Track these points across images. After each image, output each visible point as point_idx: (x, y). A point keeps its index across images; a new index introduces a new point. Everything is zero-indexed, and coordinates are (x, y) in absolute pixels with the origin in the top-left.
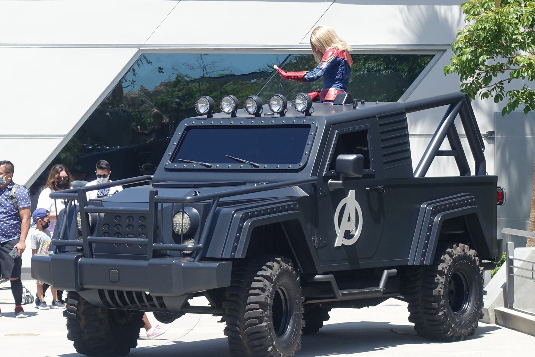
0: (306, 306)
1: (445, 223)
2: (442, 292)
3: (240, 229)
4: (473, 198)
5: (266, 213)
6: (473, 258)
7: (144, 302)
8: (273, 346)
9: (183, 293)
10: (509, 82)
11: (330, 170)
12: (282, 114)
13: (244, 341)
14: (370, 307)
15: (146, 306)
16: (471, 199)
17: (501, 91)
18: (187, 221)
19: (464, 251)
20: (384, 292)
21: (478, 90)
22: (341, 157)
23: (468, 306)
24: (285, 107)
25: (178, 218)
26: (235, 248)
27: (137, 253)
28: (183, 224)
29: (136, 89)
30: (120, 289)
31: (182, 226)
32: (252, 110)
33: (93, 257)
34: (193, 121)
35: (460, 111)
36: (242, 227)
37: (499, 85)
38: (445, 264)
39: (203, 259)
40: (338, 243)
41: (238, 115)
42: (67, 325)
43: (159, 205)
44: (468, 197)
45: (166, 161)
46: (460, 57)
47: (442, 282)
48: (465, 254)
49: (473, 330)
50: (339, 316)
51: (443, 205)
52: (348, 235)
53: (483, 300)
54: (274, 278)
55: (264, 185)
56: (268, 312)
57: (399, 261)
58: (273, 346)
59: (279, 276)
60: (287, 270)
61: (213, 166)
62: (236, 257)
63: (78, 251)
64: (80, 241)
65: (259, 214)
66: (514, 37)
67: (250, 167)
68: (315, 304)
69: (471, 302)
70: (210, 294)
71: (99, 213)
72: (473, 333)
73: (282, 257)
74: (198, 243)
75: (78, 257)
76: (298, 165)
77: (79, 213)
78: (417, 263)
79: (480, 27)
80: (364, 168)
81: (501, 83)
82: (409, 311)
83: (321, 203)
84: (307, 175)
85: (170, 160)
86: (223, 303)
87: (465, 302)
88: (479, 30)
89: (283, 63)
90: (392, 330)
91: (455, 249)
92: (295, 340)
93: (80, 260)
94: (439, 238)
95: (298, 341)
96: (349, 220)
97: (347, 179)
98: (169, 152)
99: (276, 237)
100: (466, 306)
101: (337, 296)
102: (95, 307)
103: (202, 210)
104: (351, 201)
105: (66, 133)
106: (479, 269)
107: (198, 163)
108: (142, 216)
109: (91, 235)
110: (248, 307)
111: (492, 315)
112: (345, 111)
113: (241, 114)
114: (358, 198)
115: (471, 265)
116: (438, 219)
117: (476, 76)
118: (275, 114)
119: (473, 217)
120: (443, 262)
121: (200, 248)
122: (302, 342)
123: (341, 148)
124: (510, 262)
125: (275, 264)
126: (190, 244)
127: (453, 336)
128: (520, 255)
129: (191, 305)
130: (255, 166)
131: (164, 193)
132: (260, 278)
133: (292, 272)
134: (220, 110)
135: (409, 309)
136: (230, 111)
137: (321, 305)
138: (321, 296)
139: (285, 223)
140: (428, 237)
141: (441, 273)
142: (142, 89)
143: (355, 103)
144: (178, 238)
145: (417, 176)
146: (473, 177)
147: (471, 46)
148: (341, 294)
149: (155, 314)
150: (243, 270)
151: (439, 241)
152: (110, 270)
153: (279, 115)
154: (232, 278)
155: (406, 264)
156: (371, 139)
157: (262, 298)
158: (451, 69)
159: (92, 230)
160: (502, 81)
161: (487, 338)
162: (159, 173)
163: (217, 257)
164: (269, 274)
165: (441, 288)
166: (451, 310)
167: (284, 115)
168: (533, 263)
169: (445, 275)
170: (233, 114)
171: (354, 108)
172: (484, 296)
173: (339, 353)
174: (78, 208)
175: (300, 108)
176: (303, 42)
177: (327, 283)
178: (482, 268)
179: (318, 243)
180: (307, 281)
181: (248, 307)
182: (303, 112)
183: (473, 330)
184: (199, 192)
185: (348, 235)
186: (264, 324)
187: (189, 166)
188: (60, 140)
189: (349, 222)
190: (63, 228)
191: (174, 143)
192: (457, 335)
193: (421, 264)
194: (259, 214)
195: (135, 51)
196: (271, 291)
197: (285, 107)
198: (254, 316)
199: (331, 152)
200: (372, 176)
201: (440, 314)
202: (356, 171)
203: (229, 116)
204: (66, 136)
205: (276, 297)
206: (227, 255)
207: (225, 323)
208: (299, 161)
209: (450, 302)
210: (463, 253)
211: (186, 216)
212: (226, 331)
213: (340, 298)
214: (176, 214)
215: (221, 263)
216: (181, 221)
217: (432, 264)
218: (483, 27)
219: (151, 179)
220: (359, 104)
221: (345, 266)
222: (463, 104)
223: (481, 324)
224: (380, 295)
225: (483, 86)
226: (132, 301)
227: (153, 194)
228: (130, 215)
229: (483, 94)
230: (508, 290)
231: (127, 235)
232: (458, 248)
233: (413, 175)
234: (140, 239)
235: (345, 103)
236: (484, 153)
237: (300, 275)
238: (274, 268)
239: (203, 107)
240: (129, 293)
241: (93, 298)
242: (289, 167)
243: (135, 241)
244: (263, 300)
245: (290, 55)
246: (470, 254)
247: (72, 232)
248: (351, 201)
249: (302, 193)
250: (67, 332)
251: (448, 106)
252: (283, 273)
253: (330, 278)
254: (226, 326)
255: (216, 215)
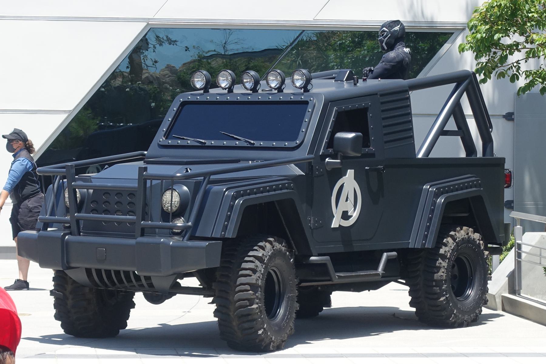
0: (300, 289)
1: (449, 205)
2: (444, 277)
3: (231, 208)
4: (478, 180)
5: (259, 191)
6: (478, 242)
7: (132, 282)
8: (264, 329)
9: (171, 272)
10: (526, 61)
11: (327, 148)
12: (280, 89)
13: (234, 324)
14: (371, 291)
15: (134, 286)
16: (477, 181)
17: (517, 71)
18: (176, 199)
19: (468, 234)
20: (383, 276)
21: (494, 69)
22: (339, 135)
23: (471, 293)
24: (283, 82)
25: (167, 196)
26: (225, 228)
27: (125, 230)
28: (172, 201)
29: (161, 66)
30: (108, 268)
31: (171, 204)
32: (249, 85)
33: (80, 235)
34: (189, 96)
35: (466, 90)
36: (233, 206)
37: (515, 64)
38: (448, 247)
39: (193, 238)
40: (335, 224)
41: (235, 91)
42: (54, 305)
43: (148, 182)
44: (474, 179)
45: (160, 138)
46: (474, 35)
47: (444, 267)
48: (469, 237)
49: (477, 316)
50: (341, 300)
51: (451, 186)
52: (345, 216)
53: (488, 286)
54: (266, 259)
55: (259, 163)
56: (259, 294)
57: (400, 244)
58: (264, 329)
59: (271, 257)
60: (280, 251)
61: (208, 143)
62: (226, 237)
63: (66, 228)
64: (68, 218)
65: (252, 192)
66: (530, 15)
67: (245, 145)
68: (313, 286)
69: (475, 288)
70: (200, 274)
71: (88, 189)
72: (476, 320)
73: (275, 237)
74: (188, 222)
75: (65, 235)
76: (295, 142)
77: (67, 189)
78: (418, 246)
79: (495, 4)
80: (363, 147)
81: (518, 62)
82: (410, 295)
83: (318, 182)
84: (303, 153)
85: (164, 137)
86: (213, 284)
87: (469, 287)
88: (494, 7)
89: (298, 37)
90: (394, 315)
91: (458, 232)
92: (288, 323)
93: (67, 237)
94: (442, 220)
95: (291, 324)
96: (347, 200)
97: (345, 158)
98: (164, 128)
99: (269, 217)
100: (469, 292)
101: (333, 279)
102: (83, 286)
103: (193, 188)
104: (349, 181)
105: (71, 108)
106: (484, 254)
107: (193, 139)
108: (132, 193)
109: (79, 212)
110: (238, 289)
111: (499, 301)
112: (346, 87)
113: (238, 90)
114: (357, 178)
115: (475, 249)
116: (441, 200)
117: (491, 54)
118: (273, 90)
119: (478, 199)
120: (446, 245)
121: (189, 227)
122: (296, 326)
123: (339, 126)
124: (519, 246)
125: (268, 245)
126: (180, 223)
127: (455, 322)
128: (530, 240)
129: (182, 285)
130: (250, 143)
131: (153, 170)
132: (251, 259)
133: (286, 253)
134: (215, 85)
135: (410, 293)
136: (227, 87)
137: (319, 288)
138: (317, 278)
139: (279, 202)
140: (430, 219)
141: (443, 257)
142: (168, 67)
143: (356, 80)
144: (167, 216)
145: (420, 156)
146: (480, 159)
147: (486, 23)
148: (338, 276)
149: (144, 294)
150: (234, 250)
151: (441, 224)
152: (97, 248)
153: (276, 91)
154: (221, 258)
155: (406, 247)
156: (371, 117)
157: (253, 279)
158: (466, 48)
159: (79, 207)
160: (519, 61)
161: (489, 325)
162: (153, 150)
163: (207, 236)
164: (260, 255)
165: (443, 272)
166: (453, 295)
167: (282, 91)
168: (541, 248)
169: (449, 259)
170: (230, 90)
171: (355, 84)
172: (489, 282)
173: (332, 337)
174: (66, 184)
175: (298, 84)
176: (317, 18)
177: (322, 266)
178: (486, 253)
179: (314, 224)
180: (301, 263)
181: (238, 289)
182: (301, 88)
183: (477, 316)
184: (190, 169)
185: (345, 216)
186: (255, 306)
187: (184, 143)
188: (64, 116)
189: (347, 202)
190: (51, 204)
191: (169, 118)
192: (460, 321)
193: (423, 247)
194: (252, 192)
195: (143, 25)
196: (262, 272)
197: (283, 82)
198: (245, 298)
199: (329, 129)
200: (372, 155)
201: (442, 299)
202: (354, 150)
203: (226, 91)
204: (71, 112)
205: (269, 279)
206: (217, 234)
207: (215, 304)
208: (296, 139)
209: (453, 287)
210: (466, 236)
211: (175, 194)
212: (216, 313)
213: (336, 281)
214: (165, 191)
215: (211, 242)
216: (171, 199)
217: (434, 247)
218: (499, 4)
219: (144, 155)
220: (360, 81)
221: (339, 248)
222: (471, 83)
223: (485, 311)
224: (379, 278)
225: (499, 65)
226: (120, 281)
227: (142, 170)
228: (119, 192)
229: (500, 73)
230: (514, 282)
231: (116, 212)
232: (462, 232)
233: (415, 155)
234: (128, 217)
235: (346, 80)
236: (492, 134)
237: (294, 256)
238: (266, 249)
239: (199, 82)
240: (117, 273)
241: (79, 276)
242: (285, 145)
243: (123, 219)
244: (254, 282)
245: (304, 31)
246: (475, 237)
247: (60, 209)
248: (349, 181)
249: (298, 172)
250: (54, 311)
251: (454, 85)
252: (276, 254)
253: (325, 260)
254: (216, 307)
255: (206, 193)
